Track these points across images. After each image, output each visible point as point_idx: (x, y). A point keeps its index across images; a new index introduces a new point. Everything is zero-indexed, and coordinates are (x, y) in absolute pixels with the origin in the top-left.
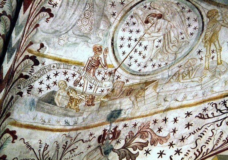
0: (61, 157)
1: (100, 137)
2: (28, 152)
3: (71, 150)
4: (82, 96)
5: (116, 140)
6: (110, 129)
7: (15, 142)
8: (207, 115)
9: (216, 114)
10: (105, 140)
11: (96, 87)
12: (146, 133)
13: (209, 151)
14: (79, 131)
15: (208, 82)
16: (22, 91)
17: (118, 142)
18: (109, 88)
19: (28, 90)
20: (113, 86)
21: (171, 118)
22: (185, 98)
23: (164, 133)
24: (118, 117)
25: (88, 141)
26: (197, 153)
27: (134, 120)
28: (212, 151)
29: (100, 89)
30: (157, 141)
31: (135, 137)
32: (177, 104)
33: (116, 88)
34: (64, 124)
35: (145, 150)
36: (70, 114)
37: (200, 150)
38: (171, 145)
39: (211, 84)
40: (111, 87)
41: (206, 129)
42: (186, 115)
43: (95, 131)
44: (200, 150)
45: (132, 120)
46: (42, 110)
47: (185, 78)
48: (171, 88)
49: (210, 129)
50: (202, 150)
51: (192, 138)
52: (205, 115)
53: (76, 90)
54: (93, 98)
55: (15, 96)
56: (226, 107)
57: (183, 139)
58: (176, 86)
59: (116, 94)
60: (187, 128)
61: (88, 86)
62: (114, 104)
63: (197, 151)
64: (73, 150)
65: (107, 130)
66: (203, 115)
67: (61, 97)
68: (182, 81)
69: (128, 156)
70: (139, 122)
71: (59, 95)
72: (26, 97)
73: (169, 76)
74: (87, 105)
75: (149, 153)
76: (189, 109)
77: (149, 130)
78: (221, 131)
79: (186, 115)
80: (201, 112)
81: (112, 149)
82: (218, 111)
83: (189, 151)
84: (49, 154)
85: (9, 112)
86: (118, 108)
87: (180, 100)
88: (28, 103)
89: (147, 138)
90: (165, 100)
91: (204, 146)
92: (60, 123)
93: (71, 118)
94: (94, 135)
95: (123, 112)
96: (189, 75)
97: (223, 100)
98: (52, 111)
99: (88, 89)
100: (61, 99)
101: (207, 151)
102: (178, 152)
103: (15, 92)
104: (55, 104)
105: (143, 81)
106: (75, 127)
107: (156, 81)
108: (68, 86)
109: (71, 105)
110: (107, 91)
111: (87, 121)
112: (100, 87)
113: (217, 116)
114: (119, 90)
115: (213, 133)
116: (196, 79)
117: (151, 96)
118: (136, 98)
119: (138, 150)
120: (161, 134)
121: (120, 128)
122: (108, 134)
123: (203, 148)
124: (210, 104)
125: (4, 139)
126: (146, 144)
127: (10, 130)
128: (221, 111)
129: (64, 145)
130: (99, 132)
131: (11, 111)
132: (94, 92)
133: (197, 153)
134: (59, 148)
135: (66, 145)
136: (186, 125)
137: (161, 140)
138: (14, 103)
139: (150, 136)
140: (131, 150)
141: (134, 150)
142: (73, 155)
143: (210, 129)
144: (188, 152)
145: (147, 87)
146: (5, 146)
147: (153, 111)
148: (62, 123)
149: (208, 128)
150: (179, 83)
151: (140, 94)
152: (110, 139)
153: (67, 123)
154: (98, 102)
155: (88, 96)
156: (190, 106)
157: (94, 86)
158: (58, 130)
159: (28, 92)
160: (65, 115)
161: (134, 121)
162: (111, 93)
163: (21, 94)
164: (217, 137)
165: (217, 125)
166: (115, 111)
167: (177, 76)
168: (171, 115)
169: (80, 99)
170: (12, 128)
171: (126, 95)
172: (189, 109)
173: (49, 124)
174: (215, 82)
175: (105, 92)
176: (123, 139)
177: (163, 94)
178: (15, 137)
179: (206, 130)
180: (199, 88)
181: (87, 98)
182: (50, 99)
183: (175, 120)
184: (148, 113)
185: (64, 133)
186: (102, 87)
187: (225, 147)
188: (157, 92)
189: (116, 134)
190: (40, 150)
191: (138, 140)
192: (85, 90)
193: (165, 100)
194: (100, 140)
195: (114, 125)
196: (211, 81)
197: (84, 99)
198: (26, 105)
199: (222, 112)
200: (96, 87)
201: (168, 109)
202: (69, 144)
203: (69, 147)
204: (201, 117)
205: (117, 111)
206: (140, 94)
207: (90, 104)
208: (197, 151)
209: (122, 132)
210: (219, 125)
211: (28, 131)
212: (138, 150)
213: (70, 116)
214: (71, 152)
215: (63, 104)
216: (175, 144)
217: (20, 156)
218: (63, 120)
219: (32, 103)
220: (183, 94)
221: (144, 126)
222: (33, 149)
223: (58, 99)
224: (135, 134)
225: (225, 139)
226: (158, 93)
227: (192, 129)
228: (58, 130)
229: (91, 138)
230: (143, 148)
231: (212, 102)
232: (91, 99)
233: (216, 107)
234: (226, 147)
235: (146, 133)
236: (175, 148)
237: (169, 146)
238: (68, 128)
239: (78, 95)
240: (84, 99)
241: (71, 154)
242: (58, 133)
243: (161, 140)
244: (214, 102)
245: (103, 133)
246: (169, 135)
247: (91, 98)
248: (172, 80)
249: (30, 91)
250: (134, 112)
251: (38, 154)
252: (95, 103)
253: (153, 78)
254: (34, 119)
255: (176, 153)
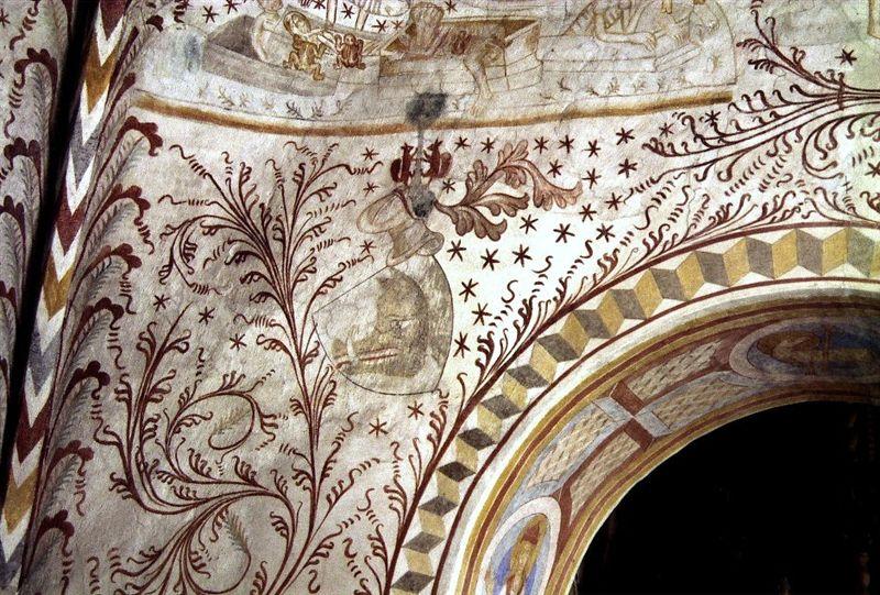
0: (296, 207)
1: (395, 167)
2: (197, 184)
3: (320, 190)
4: (326, 34)
5: (442, 180)
6: (421, 146)
7: (157, 154)
8: (671, 145)
9: (693, 146)
10: (412, 176)
11: (363, 13)
12: (520, 174)
13: (677, 240)
14: (332, 140)
15: (672, 51)
16: (160, 13)
17: (448, 187)
18: (400, 19)
19: (175, 13)
20: (411, 15)
21: (581, 144)
22: (614, 88)
23: (566, 180)
24: (438, 116)
25: (363, 173)
26: (651, 243)
27: (484, 129)
28: (685, 239)
29: (373, 20)
30: (550, 197)
31: (490, 179)
32: (594, 103)
33: (420, 25)
34: (285, 114)
35: (523, 219)
36: (301, 86)
37: (656, 235)
38: (587, 212)
39: (680, 60)
40: (404, 18)
41: (669, 182)
42: (620, 137)
43: (380, 146)
44: (656, 235)
45: (478, 129)
46: (221, 70)
47: (612, 29)
48: (577, 54)
49: (679, 183)
50: (661, 235)
51: (637, 202)
52: (665, 145)
53: (308, 16)
54: (357, 46)
55: (142, 28)
56: (716, 130)
57: (614, 202)
58: (589, 50)
59: (422, 43)
60: (624, 174)
61: (341, 7)
62: (421, 75)
63: (651, 235)
64: (324, 190)
65: (412, 148)
66: (662, 145)
67: (267, 35)
68: (604, 37)
69: (479, 227)
70: (496, 139)
71: (262, 29)
72: (171, 30)
73: (568, 15)
74: (344, 63)
75: (516, 253)
76: (629, 123)
77: (526, 165)
78: (705, 192)
79: (620, 137)
80: (657, 136)
81: (435, 203)
82: (699, 140)
83: (631, 233)
84: (258, 191)
85: (130, 71)
86: (436, 90)
87: (602, 93)
88: (180, 49)
89: (523, 187)
90: (563, 88)
91: (666, 227)
92: (275, 109)
93: (302, 99)
94: (378, 158)
95: (449, 102)
96: (622, 23)
97: (707, 109)
98: (248, 74)
99: (341, 15)
100: (268, 39)
101: (673, 238)
102: (605, 233)
103: (140, 18)
104: (255, 56)
105: (497, 16)
106: (318, 125)
107: (533, 21)
108: (285, 6)
109: (297, 60)
110: (396, 28)
111: (352, 113)
112: (373, 12)
113: (696, 153)
114: (429, 31)
115: (686, 195)
116: (640, 38)
117: (522, 66)
118: (483, 66)
119: (503, 216)
120: (558, 181)
121: (447, 147)
122: (416, 160)
123: (664, 230)
124: (676, 116)
125: (126, 145)
126: (522, 203)
127: (141, 121)
128: (704, 140)
129: (295, 173)
130: (390, 151)
131: (135, 70)
132: (359, 27)
133: (651, 243)
134: (283, 181)
135: (300, 172)
136: (621, 165)
137: (560, 197)
138: (141, 47)
139: (530, 182)
140: (485, 212)
141: (495, 214)
142: (330, 206)
143: (679, 183)
144: (628, 236)
145: (510, 38)
146: (134, 163)
147: (533, 112)
148: (281, 109)
149: (673, 181)
150: (597, 41)
151: (493, 56)
152: (424, 176)
153: (293, 111)
154: (374, 58)
155: (342, 36)
156: (627, 112)
157: (355, 10)
158: (270, 129)
159: (177, 15)
160: (286, 89)
161: (483, 134)
162: (408, 36)
163: (156, 22)
164: (695, 206)
165: (696, 176)
166: (428, 95)
167: (590, 17)
168: (582, 132)
169: (322, 43)
170: (146, 117)
171: (453, 52)
172: (629, 123)
173: (245, 109)
174: (690, 55)
175: (390, 31)
176: (461, 180)
177: (557, 68)
178: (156, 142)
179: (669, 186)
180: (648, 65)
181: (341, 44)
182: (238, 40)
183: (593, 149)
184: (519, 117)
185: (290, 138)
186: (379, 14)
187: (721, 231)
188: (540, 58)
189: (439, 164)
190: (229, 179)
191: (500, 186)
192: (331, 19)
193: (563, 88)
194: (397, 175)
195: (430, 136)
196: (680, 52)
197: (333, 46)
198: (174, 54)
199: (706, 144)
200: (363, 13)
201: (571, 114)
202: (308, 172)
203: (312, 180)
204: (656, 148)
205: (432, 96)
206: (493, 56)
207: (351, 61)
208: (651, 235)
209: (455, 161)
210: (700, 177)
211: (189, 126)
212: (503, 216)
213: (300, 93)
214: (321, 196)
215: (278, 57)
216: (595, 212)
217: (176, 192)
218: (281, 101)
219: (192, 49)
220: (609, 76)
221: (512, 153)
222: (211, 177)
223: (261, 41)
224: (490, 171)
225: (714, 215)
226: (542, 63)
227: (635, 179)
228: (270, 129)
229: (370, 164)
230: (516, 211)
231: (681, 111)
232: (351, 47)
233: (693, 128)
234: (715, 233)
235: (520, 174)
236: (597, 222)
237: (582, 216)
238: (299, 124)
239: (315, 31)
240: (333, 46)
241: (322, 201)
242: (272, 137)
243: (562, 196)
244: (688, 111)
245: (402, 155)
246: (579, 186)
247: (351, 43)
248: (576, 28)
249: (182, 13)
250: (480, 105)
251: (225, 189)
252: (366, 60)
253: (522, 13)
254: (200, 94)
255: (600, 236)
